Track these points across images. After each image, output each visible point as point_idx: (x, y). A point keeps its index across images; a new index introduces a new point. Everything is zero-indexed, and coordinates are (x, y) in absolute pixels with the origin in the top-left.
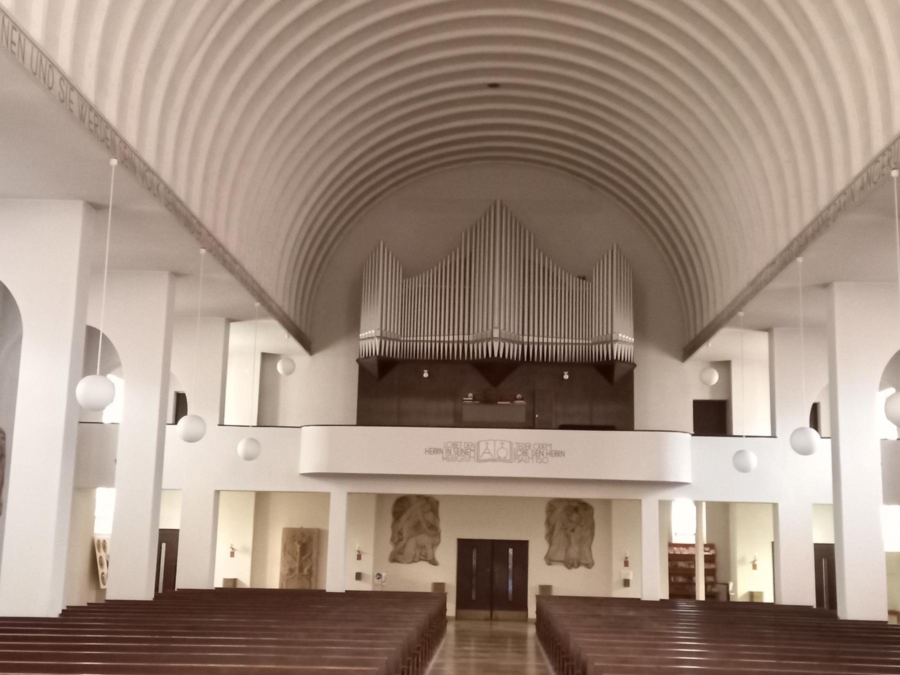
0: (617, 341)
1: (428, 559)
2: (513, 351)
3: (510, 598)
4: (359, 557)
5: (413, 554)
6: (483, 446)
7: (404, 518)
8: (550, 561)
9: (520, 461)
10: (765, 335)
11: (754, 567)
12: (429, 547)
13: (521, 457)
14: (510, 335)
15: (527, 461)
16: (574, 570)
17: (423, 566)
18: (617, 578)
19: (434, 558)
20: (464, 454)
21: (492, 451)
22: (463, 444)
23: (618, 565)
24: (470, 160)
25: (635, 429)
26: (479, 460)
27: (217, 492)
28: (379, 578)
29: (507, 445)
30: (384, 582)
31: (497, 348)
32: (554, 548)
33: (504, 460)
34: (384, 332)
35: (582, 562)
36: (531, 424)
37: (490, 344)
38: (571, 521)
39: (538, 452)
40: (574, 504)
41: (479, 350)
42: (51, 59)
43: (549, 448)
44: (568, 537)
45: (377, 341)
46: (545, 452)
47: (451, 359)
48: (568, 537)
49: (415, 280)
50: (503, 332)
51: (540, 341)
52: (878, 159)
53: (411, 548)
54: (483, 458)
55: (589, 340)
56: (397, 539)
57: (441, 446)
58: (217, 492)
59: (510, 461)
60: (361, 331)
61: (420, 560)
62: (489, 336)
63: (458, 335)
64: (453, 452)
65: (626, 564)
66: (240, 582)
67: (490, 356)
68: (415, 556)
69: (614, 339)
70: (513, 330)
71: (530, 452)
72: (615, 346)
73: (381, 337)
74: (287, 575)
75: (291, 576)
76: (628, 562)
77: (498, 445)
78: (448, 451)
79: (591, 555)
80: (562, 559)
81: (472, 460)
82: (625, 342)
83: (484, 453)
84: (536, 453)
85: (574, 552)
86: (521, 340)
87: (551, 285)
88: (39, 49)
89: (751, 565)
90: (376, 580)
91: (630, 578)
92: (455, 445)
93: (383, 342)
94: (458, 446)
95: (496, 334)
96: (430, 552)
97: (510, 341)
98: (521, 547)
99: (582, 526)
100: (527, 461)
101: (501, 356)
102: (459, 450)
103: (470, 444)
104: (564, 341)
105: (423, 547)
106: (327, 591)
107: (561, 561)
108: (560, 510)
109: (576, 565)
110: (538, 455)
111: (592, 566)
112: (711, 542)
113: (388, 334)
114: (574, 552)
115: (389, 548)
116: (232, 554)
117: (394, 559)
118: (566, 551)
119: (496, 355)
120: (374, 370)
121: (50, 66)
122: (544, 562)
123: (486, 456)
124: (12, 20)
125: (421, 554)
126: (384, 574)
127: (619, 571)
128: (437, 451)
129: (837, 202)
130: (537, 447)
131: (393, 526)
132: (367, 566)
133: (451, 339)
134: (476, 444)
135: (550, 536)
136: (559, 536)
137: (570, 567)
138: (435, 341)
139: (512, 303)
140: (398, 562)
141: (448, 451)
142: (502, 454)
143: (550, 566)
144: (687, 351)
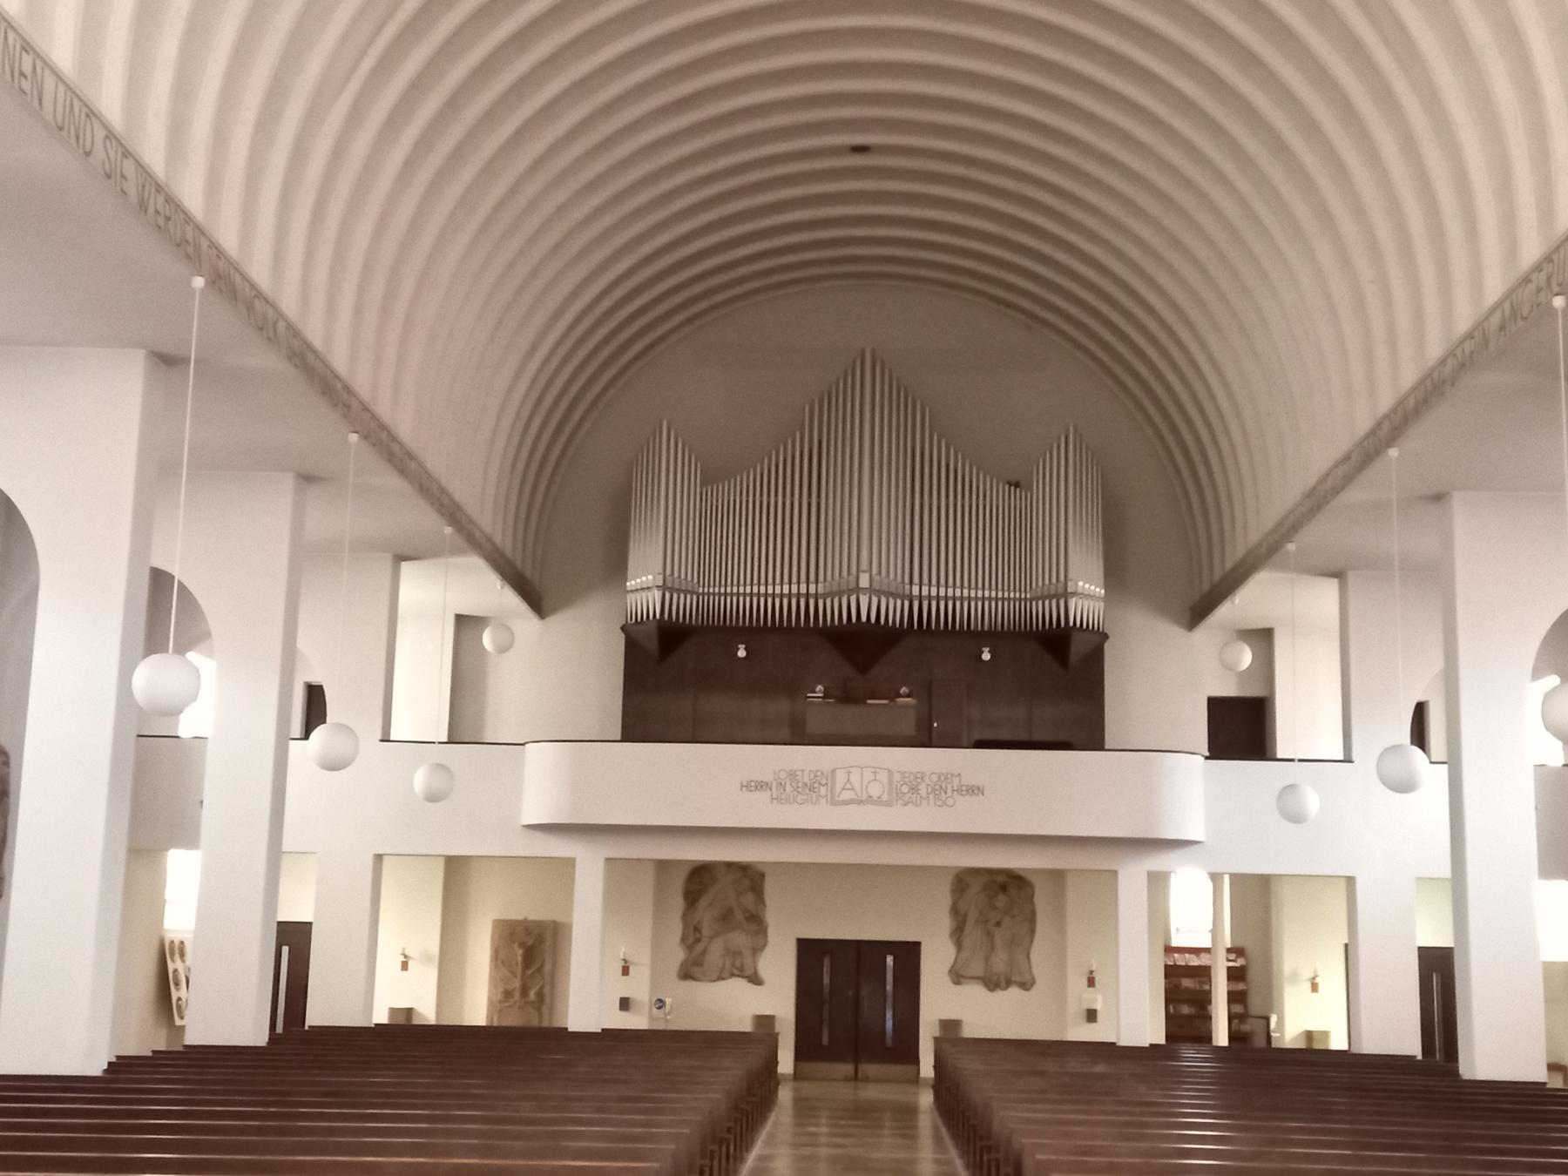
0: (1074, 594)
1: (746, 974)
2: (894, 611)
3: (889, 1042)
4: (626, 971)
5: (720, 964)
6: (841, 778)
7: (703, 903)
8: (957, 977)
9: (906, 804)
10: (1333, 584)
11: (1314, 988)
12: (747, 953)
13: (908, 796)
14: (889, 584)
15: (919, 803)
16: (999, 994)
17: (737, 986)
18: (1074, 1008)
19: (756, 973)
20: (808, 792)
21: (857, 786)
22: (806, 773)
23: (1076, 984)
24: (818, 279)
25: (1107, 747)
26: (834, 802)
27: (379, 858)
28: (660, 1008)
29: (883, 776)
30: (669, 1013)
31: (866, 606)
32: (965, 954)
33: (878, 802)
34: (669, 579)
35: (1013, 979)
36: (925, 738)
37: (853, 599)
38: (995, 908)
39: (937, 787)
40: (1001, 879)
41: (834, 611)
42: (89, 103)
43: (956, 781)
44: (990, 935)
45: (657, 594)
46: (949, 787)
47: (785, 625)
48: (990, 935)
49: (723, 488)
50: (876, 578)
51: (940, 595)
52: (1530, 277)
53: (715, 954)
54: (842, 797)
55: (1026, 592)
56: (691, 940)
57: (768, 778)
58: (379, 858)
59: (888, 804)
60: (629, 576)
61: (732, 975)
62: (852, 586)
63: (799, 583)
64: (788, 788)
65: (1091, 982)
66: (419, 1013)
67: (854, 620)
68: (723, 968)
69: (1069, 590)
70: (894, 574)
71: (923, 788)
72: (1072, 603)
73: (663, 588)
74: (500, 1002)
75: (507, 1004)
76: (1094, 978)
77: (868, 775)
78: (781, 785)
79: (1030, 967)
80: (979, 973)
81: (823, 801)
82: (1089, 596)
83: (843, 789)
84: (934, 790)
85: (999, 962)
86: (907, 592)
87: (959, 497)
88: (68, 86)
89: (1309, 985)
90: (655, 1010)
91: (1098, 1006)
92: (792, 775)
93: (668, 596)
94: (798, 778)
95: (864, 582)
96: (748, 961)
97: (888, 594)
98: (909, 953)
99: (1013, 917)
100: (919, 803)
101: (873, 620)
102: (800, 785)
103: (819, 774)
104: (983, 595)
105: (737, 953)
106: (569, 1030)
107: (978, 978)
108: (975, 888)
109: (1003, 984)
110: (937, 792)
111: (1032, 985)
112: (1239, 944)
113: (677, 581)
114: (999, 962)
115: (678, 955)
116: (405, 966)
117: (686, 974)
118: (987, 960)
119: (864, 619)
120: (652, 645)
121: (87, 115)
122: (947, 980)
123: (847, 795)
124: (20, 35)
125: (733, 965)
126: (668, 1001)
127: (1079, 995)
128: (761, 786)
129: (1459, 352)
130: (935, 778)
131: (685, 917)
132: (639, 987)
133: (786, 591)
134: (830, 774)
135: (958, 934)
136: (973, 934)
137: (992, 987)
138: (759, 593)
139: (892, 528)
140: (693, 978)
141: (781, 785)
142: (875, 790)
143: (958, 987)
144: (1197, 612)
